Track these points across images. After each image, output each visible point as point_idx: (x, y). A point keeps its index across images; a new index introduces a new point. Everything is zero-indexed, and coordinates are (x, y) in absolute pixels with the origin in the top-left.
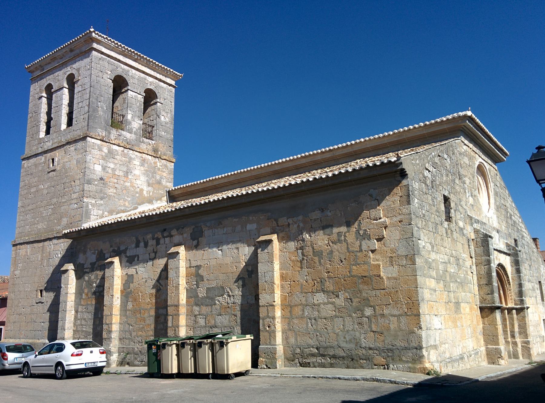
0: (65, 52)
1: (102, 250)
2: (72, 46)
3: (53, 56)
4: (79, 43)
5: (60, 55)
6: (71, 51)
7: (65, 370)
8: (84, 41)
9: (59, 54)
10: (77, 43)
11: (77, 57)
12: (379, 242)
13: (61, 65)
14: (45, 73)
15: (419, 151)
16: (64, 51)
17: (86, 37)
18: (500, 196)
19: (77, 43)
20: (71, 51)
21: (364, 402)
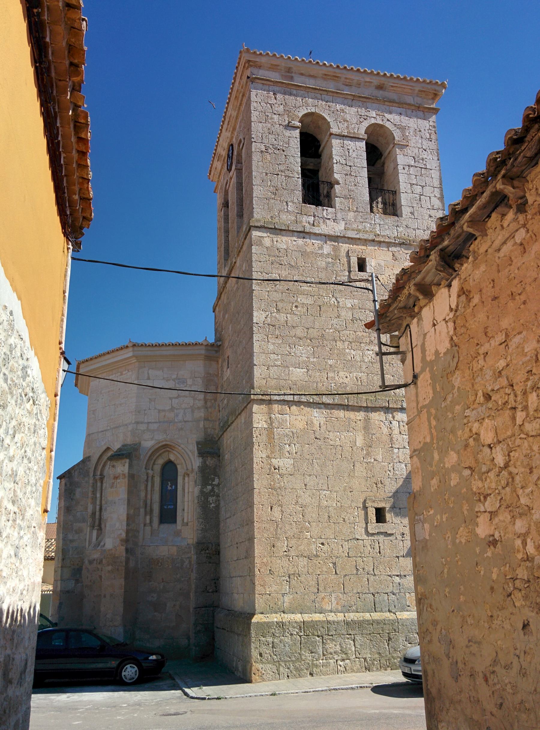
0: (366, 82)
1: (369, 326)
2: (389, 82)
3: (335, 72)
4: (406, 87)
5: (352, 80)
6: (380, 87)
7: (216, 342)
8: (420, 91)
9: (353, 77)
10: (403, 84)
11: (397, 105)
12: (363, 257)
13: (349, 97)
14: (302, 89)
15: (291, 175)
16: (368, 79)
17: (429, 87)
18: (470, 275)
19: (403, 84)
20: (380, 87)
21: (50, 156)
